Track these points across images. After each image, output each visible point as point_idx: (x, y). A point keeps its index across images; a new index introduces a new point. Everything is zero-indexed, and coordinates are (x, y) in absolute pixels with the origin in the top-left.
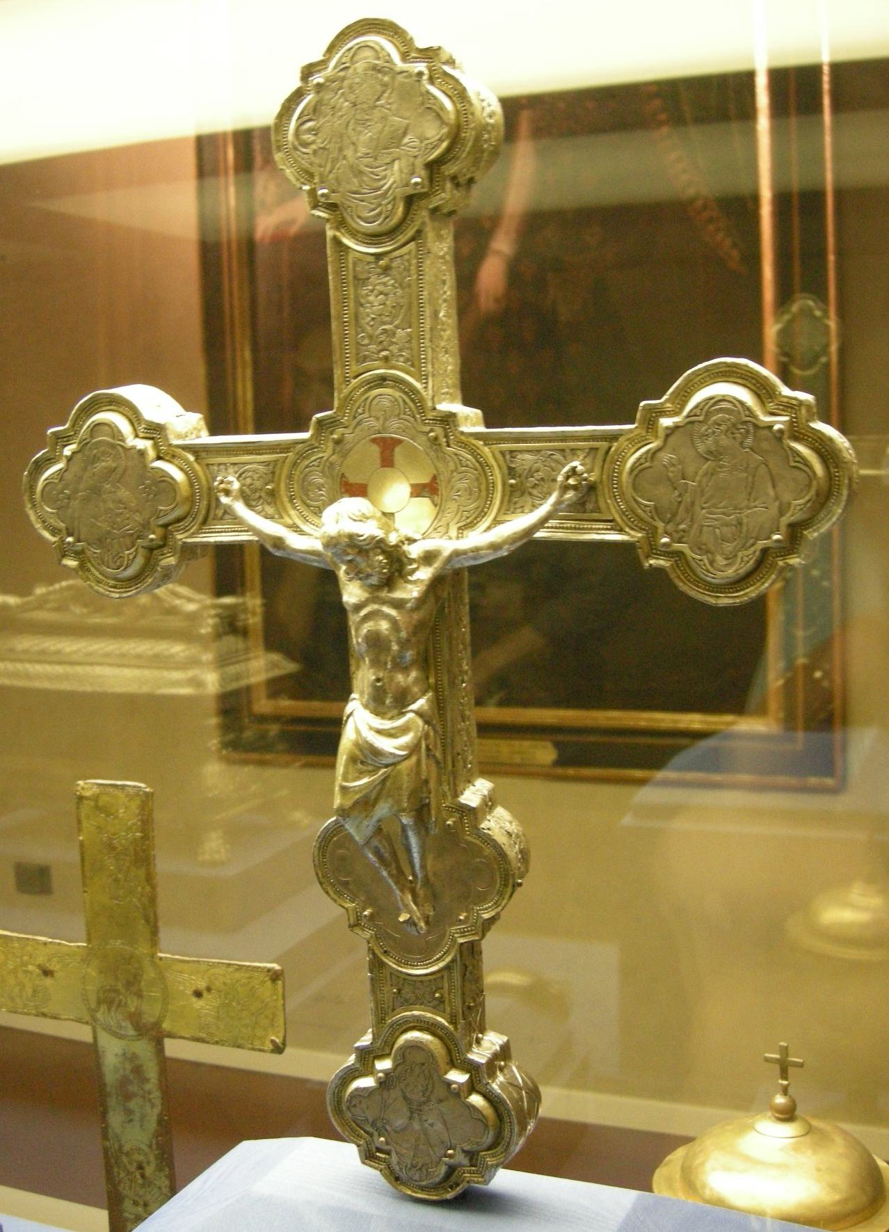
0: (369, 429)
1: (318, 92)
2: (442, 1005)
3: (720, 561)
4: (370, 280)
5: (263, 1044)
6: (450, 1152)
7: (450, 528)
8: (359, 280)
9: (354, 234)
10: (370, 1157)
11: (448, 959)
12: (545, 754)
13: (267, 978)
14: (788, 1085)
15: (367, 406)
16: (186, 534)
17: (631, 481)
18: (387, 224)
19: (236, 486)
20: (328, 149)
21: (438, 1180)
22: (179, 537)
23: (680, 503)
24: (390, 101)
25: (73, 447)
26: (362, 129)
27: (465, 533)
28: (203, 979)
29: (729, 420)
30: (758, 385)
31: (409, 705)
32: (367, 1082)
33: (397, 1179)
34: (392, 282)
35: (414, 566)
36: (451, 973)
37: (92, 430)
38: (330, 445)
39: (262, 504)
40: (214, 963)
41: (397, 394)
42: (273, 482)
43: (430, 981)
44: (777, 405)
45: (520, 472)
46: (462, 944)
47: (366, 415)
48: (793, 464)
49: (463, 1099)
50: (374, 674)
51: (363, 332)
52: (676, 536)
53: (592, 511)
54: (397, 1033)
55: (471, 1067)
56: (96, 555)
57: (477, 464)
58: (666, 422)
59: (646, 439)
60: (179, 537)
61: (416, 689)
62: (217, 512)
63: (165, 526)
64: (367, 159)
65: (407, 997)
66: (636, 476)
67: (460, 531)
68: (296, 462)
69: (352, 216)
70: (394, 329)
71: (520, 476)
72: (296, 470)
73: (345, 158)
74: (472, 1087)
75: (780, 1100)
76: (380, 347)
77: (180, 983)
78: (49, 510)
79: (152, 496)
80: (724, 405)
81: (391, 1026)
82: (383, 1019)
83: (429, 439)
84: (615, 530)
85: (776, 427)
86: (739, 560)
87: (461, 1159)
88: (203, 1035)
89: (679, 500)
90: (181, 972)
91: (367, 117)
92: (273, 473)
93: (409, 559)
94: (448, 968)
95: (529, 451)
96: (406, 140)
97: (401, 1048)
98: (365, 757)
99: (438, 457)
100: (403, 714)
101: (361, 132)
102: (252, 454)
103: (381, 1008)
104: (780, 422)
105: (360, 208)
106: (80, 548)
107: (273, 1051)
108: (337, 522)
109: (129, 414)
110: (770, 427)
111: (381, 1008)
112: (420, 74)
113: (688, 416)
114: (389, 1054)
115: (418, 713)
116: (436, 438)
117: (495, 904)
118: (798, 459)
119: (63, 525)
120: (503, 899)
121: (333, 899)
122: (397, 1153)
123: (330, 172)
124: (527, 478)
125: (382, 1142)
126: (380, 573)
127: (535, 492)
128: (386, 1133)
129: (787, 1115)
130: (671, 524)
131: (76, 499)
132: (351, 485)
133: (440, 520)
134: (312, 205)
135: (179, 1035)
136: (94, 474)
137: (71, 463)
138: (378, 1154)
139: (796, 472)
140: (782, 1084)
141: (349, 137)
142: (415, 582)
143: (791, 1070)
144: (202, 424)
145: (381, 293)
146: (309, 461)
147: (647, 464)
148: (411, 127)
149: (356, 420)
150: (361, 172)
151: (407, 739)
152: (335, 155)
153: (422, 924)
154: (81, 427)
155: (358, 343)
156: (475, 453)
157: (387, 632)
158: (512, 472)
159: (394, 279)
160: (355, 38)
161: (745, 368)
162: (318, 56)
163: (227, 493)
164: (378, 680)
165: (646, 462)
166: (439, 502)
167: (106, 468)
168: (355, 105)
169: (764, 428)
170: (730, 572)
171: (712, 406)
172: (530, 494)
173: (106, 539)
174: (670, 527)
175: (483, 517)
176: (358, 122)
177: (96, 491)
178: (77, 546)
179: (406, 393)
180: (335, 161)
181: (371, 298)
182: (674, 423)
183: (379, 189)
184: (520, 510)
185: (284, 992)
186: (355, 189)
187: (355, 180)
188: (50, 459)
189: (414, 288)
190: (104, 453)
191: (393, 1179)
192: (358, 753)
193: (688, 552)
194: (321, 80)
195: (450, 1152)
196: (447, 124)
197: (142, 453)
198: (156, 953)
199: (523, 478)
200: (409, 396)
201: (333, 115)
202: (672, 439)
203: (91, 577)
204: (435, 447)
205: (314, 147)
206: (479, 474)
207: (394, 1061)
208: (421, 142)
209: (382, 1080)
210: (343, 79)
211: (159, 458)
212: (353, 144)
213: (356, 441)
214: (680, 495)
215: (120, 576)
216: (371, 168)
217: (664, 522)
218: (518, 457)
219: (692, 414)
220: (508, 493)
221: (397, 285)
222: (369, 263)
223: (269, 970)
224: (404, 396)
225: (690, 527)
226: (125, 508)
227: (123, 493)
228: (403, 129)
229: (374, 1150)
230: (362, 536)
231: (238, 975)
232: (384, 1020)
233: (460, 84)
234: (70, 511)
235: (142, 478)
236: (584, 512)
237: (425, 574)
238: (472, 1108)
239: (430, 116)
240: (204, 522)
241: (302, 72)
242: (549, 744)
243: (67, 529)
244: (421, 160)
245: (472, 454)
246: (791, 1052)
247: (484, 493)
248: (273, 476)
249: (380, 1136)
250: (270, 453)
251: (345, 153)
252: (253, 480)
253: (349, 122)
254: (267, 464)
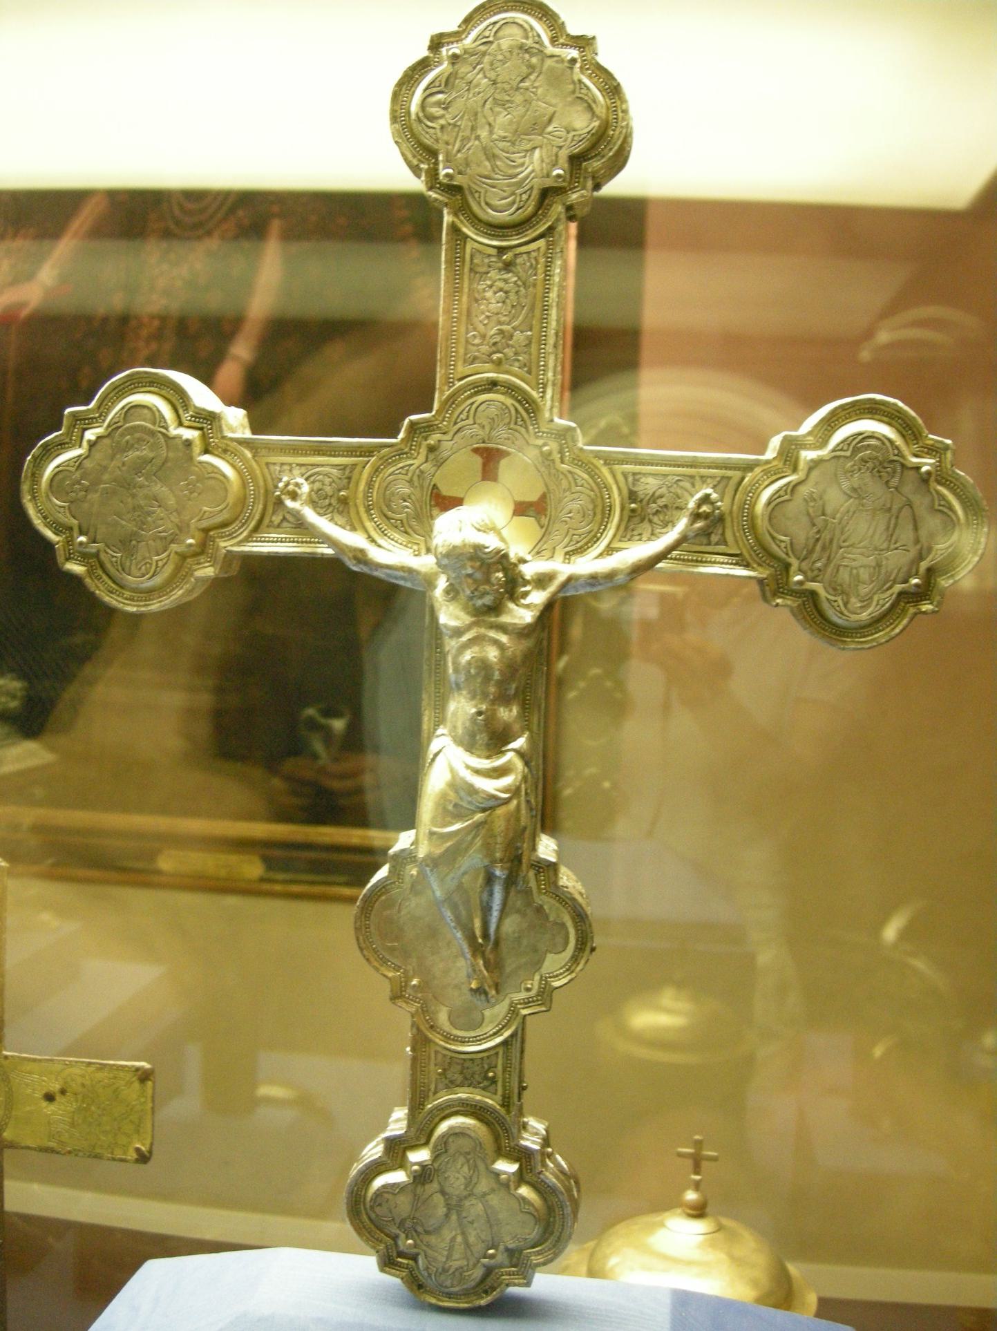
0: (472, 437)
1: (453, 64)
4: (489, 275)
5: (125, 1153)
6: (491, 1251)
7: (556, 554)
9: (476, 221)
10: (390, 1263)
11: (507, 1034)
13: (134, 1079)
14: (700, 1180)
15: (472, 412)
18: (520, 214)
19: (306, 488)
20: (459, 126)
21: (473, 1284)
22: (222, 544)
23: (818, 540)
24: (536, 84)
26: (501, 110)
27: (573, 558)
28: (56, 1080)
29: (876, 458)
30: (904, 425)
31: (509, 743)
32: (398, 1177)
33: (420, 1286)
34: (516, 279)
35: (528, 588)
36: (508, 1049)
37: (127, 412)
38: (423, 451)
39: (332, 512)
40: (70, 1061)
41: (509, 401)
42: (348, 488)
44: (922, 447)
45: (642, 496)
47: (470, 421)
48: (937, 507)
50: (476, 706)
51: (475, 329)
52: (810, 574)
53: (717, 544)
54: (437, 1119)
56: (114, 559)
57: (593, 485)
58: (807, 455)
59: (783, 472)
60: (222, 544)
62: (274, 518)
63: (206, 531)
64: (504, 143)
65: (454, 1078)
66: (773, 509)
67: (568, 557)
68: (379, 468)
69: (479, 203)
70: (512, 330)
72: (377, 476)
73: (478, 138)
74: (520, 1178)
75: (691, 1196)
76: (494, 349)
77: (27, 1085)
78: (58, 503)
79: (196, 494)
80: (873, 442)
82: (422, 1104)
83: (542, 453)
84: (740, 566)
85: (924, 469)
87: (501, 1258)
88: (52, 1144)
89: (818, 536)
90: (30, 1073)
91: (507, 98)
92: (349, 478)
93: (524, 579)
94: (505, 1043)
95: (654, 475)
96: (550, 129)
97: (443, 1136)
99: (550, 473)
100: (503, 753)
101: (499, 113)
102: (324, 455)
104: (927, 464)
105: (488, 194)
106: (94, 551)
107: (137, 1161)
108: (460, 530)
109: (173, 400)
110: (918, 468)
111: (421, 1091)
112: (573, 61)
113: (834, 450)
114: (427, 1143)
115: (518, 752)
116: (550, 453)
117: (567, 970)
119: (75, 522)
121: (374, 967)
122: (426, 1256)
123: (459, 151)
124: (648, 504)
126: (497, 590)
127: (655, 519)
128: (414, 1234)
129: (699, 1212)
130: (806, 561)
132: (444, 498)
133: (545, 543)
134: (429, 185)
135: (23, 1145)
136: (124, 464)
137: (94, 449)
138: (399, 1260)
141: (485, 117)
142: (527, 606)
143: (704, 1164)
144: (246, 421)
145: (501, 290)
146: (394, 468)
147: (786, 497)
148: (557, 115)
150: (494, 156)
151: (507, 781)
152: (467, 133)
155: (467, 341)
156: (593, 473)
157: (495, 660)
159: (517, 276)
160: (495, 14)
161: (894, 407)
162: (452, 26)
163: (294, 496)
164: (479, 713)
165: (786, 494)
166: (546, 523)
167: (139, 458)
168: (494, 83)
169: (912, 468)
170: (865, 616)
171: (857, 444)
172: (650, 521)
174: (805, 565)
175: (595, 542)
176: (496, 101)
177: (126, 485)
178: (92, 547)
179: (520, 402)
180: (465, 140)
181: (489, 294)
182: (818, 456)
183: (515, 176)
184: (638, 537)
186: (486, 173)
187: (487, 163)
188: (64, 444)
189: (540, 288)
191: (415, 1288)
192: (452, 795)
193: (822, 593)
194: (458, 51)
195: (491, 1251)
196: (598, 118)
197: (188, 443)
200: (523, 406)
201: (468, 90)
202: (815, 474)
203: (100, 585)
204: (547, 463)
205: (442, 122)
206: (596, 495)
208: (568, 132)
210: (484, 54)
212: (490, 125)
214: (818, 532)
215: (144, 586)
216: (508, 153)
217: (798, 559)
218: (642, 480)
219: (838, 448)
220: (626, 518)
221: (519, 283)
222: (489, 256)
223: (137, 1069)
224: (517, 405)
225: (826, 565)
226: (160, 506)
228: (547, 117)
229: (395, 1255)
231: (99, 1075)
232: (423, 1105)
233: (614, 79)
234: (86, 505)
236: (709, 544)
237: (538, 598)
238: (523, 1199)
239: (580, 107)
240: (256, 529)
241: (432, 41)
244: (567, 152)
245: (589, 474)
247: (599, 517)
248: (349, 483)
249: (407, 1238)
250: (346, 456)
251: (479, 132)
252: (323, 484)
253: (486, 101)
254: (343, 468)
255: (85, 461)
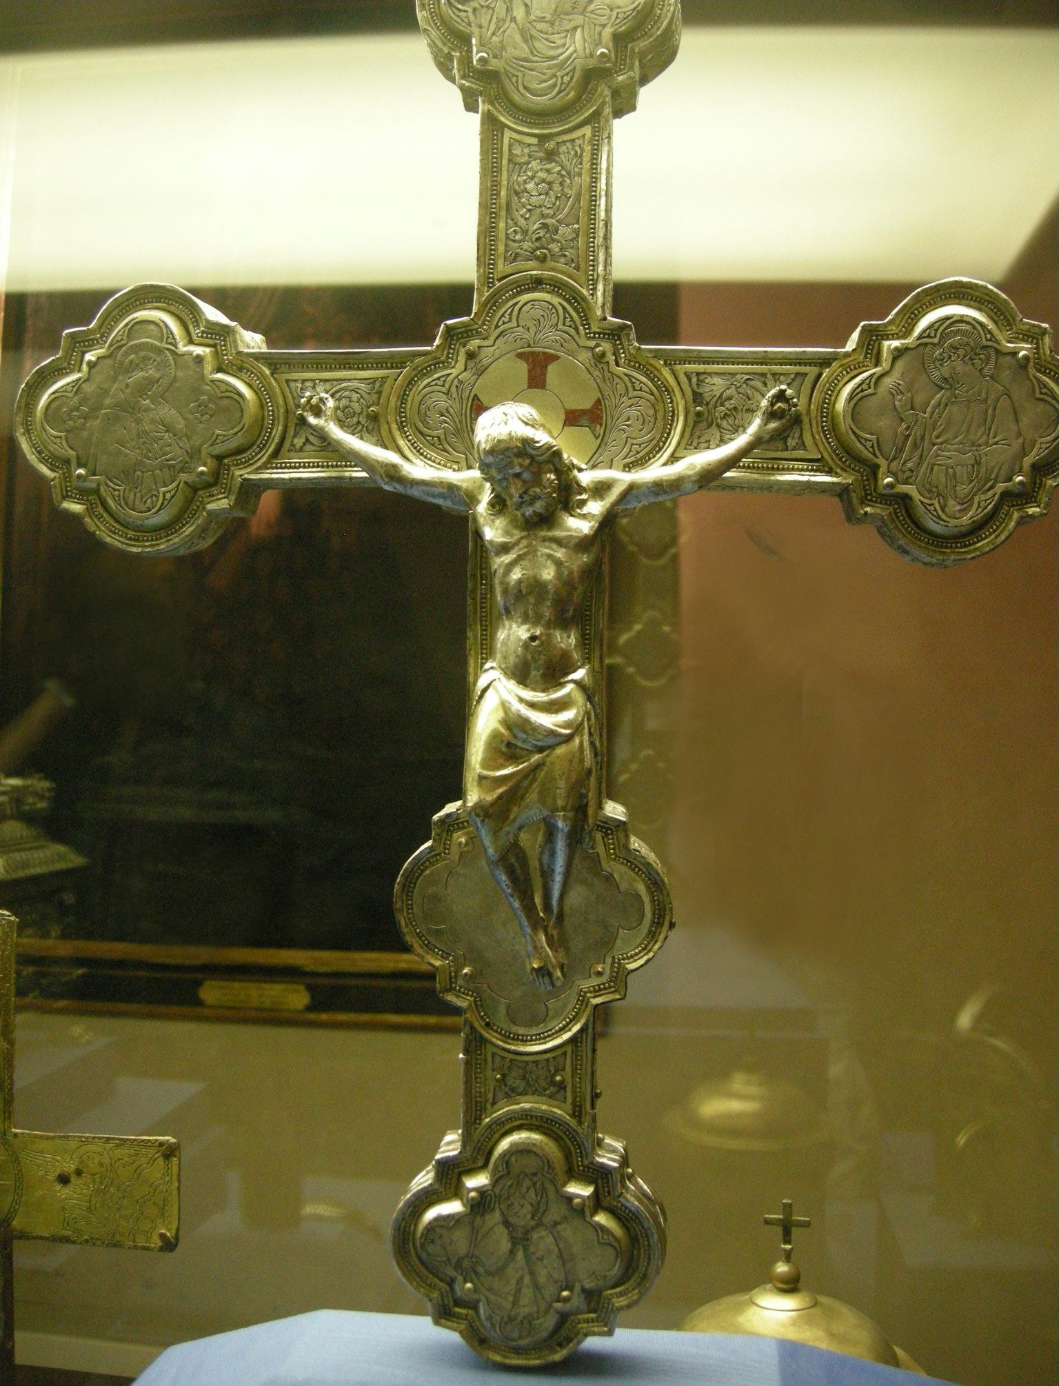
2: (562, 1092)
3: (953, 506)
6: (565, 1293)
8: (516, 164)
12: (297, 998)
15: (515, 313)
16: (249, 470)
17: (850, 410)
18: (562, 98)
21: (544, 1334)
22: (238, 473)
23: (908, 436)
25: (100, 352)
29: (967, 344)
31: (569, 673)
32: (453, 1207)
33: (483, 1341)
35: (584, 496)
36: (577, 1047)
38: (462, 358)
41: (556, 300)
42: (378, 405)
43: (548, 1060)
44: (1016, 333)
46: (597, 1006)
49: (588, 1219)
53: (794, 449)
54: (497, 1136)
55: (599, 1176)
59: (864, 366)
61: (575, 656)
63: (219, 458)
68: (413, 379)
71: (707, 404)
73: (514, 19)
74: (597, 1202)
75: (782, 1268)
80: (963, 327)
81: (489, 1126)
86: (976, 505)
87: (578, 1301)
92: (379, 393)
98: (515, 737)
100: (562, 685)
103: (476, 1102)
110: (1014, 354)
111: (476, 1102)
113: (919, 338)
114: (485, 1166)
116: (603, 354)
118: (1044, 391)
120: (656, 942)
125: (469, 1289)
127: (724, 424)
129: (790, 1286)
131: (97, 418)
137: (94, 371)
138: (457, 1310)
139: (1042, 405)
140: (785, 1250)
143: (794, 1231)
146: (430, 379)
149: (498, 331)
153: (559, 973)
154: (111, 330)
158: (697, 398)
163: (318, 412)
170: (965, 520)
172: (719, 426)
173: (135, 471)
178: (91, 481)
184: (706, 445)
185: (179, 1171)
190: (145, 359)
191: (476, 1344)
192: (503, 730)
195: (565, 1293)
197: (199, 360)
198: (9, 1128)
199: (711, 406)
207: (493, 1174)
209: (475, 1202)
211: (220, 370)
213: (497, 356)
217: (887, 459)
218: (707, 381)
223: (161, 1144)
224: (565, 304)
225: (919, 465)
226: (167, 431)
227: (167, 412)
229: (451, 1304)
230: (538, 442)
235: (197, 391)
237: (596, 508)
242: (301, 988)
243: (78, 458)
246: (794, 1209)
247: (660, 424)
249: (465, 1281)
254: (373, 381)
255: (83, 385)
